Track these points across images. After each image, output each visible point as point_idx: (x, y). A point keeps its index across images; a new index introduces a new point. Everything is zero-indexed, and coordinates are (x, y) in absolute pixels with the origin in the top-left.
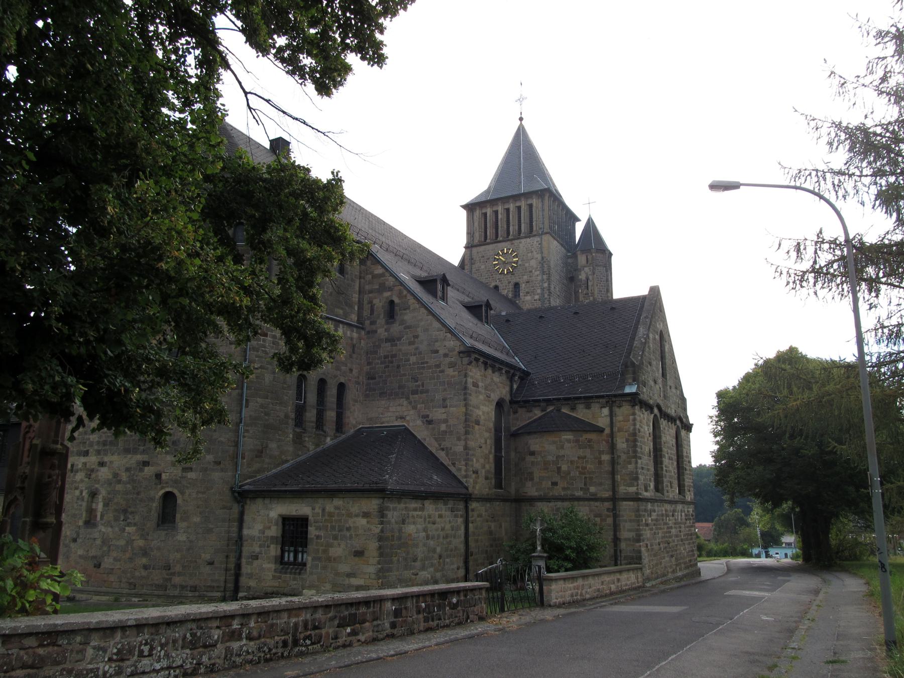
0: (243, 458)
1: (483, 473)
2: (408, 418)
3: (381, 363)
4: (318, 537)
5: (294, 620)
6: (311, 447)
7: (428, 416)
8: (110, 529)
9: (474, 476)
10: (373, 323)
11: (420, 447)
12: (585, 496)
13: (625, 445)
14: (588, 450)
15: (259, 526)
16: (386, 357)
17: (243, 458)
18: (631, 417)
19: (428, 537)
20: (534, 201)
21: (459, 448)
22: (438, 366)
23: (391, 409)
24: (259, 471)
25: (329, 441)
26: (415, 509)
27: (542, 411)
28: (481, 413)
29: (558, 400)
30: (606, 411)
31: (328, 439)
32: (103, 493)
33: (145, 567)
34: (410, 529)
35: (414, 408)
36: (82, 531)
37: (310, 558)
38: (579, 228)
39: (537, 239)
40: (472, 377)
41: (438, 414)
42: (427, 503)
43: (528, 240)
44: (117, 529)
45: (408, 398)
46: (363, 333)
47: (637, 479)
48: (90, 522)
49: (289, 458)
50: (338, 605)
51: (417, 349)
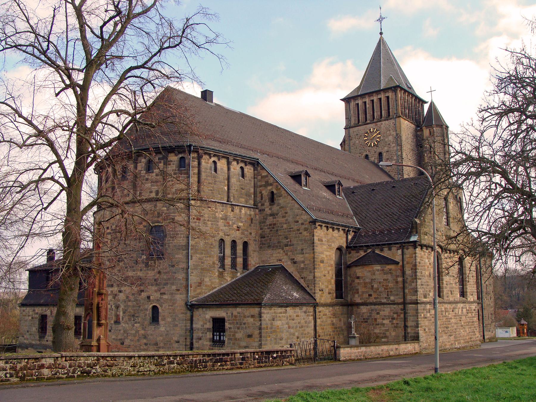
0: (191, 287)
1: (326, 291)
2: (283, 260)
3: (268, 229)
4: (230, 328)
5: (194, 359)
6: (229, 279)
7: (294, 259)
8: (127, 325)
9: (320, 292)
10: (263, 205)
11: (290, 277)
12: (388, 302)
13: (410, 272)
14: (390, 275)
15: (201, 323)
16: (270, 225)
17: (191, 287)
18: (414, 255)
19: (289, 327)
20: (390, 94)
21: (311, 277)
22: (298, 230)
23: (274, 255)
24: (200, 294)
25: (239, 275)
26: (281, 313)
27: (365, 252)
28: (324, 256)
29: (373, 245)
30: (400, 252)
31: (239, 274)
32: (122, 306)
33: (146, 344)
34: (278, 323)
35: (287, 254)
36: (113, 326)
37: (226, 339)
38: (426, 107)
39: (393, 121)
40: (317, 236)
41: (299, 258)
42: (288, 309)
43: (387, 122)
44: (130, 325)
45: (283, 249)
46: (257, 210)
47: (416, 291)
48: (117, 322)
49: (216, 286)
50: (214, 355)
51: (287, 220)
